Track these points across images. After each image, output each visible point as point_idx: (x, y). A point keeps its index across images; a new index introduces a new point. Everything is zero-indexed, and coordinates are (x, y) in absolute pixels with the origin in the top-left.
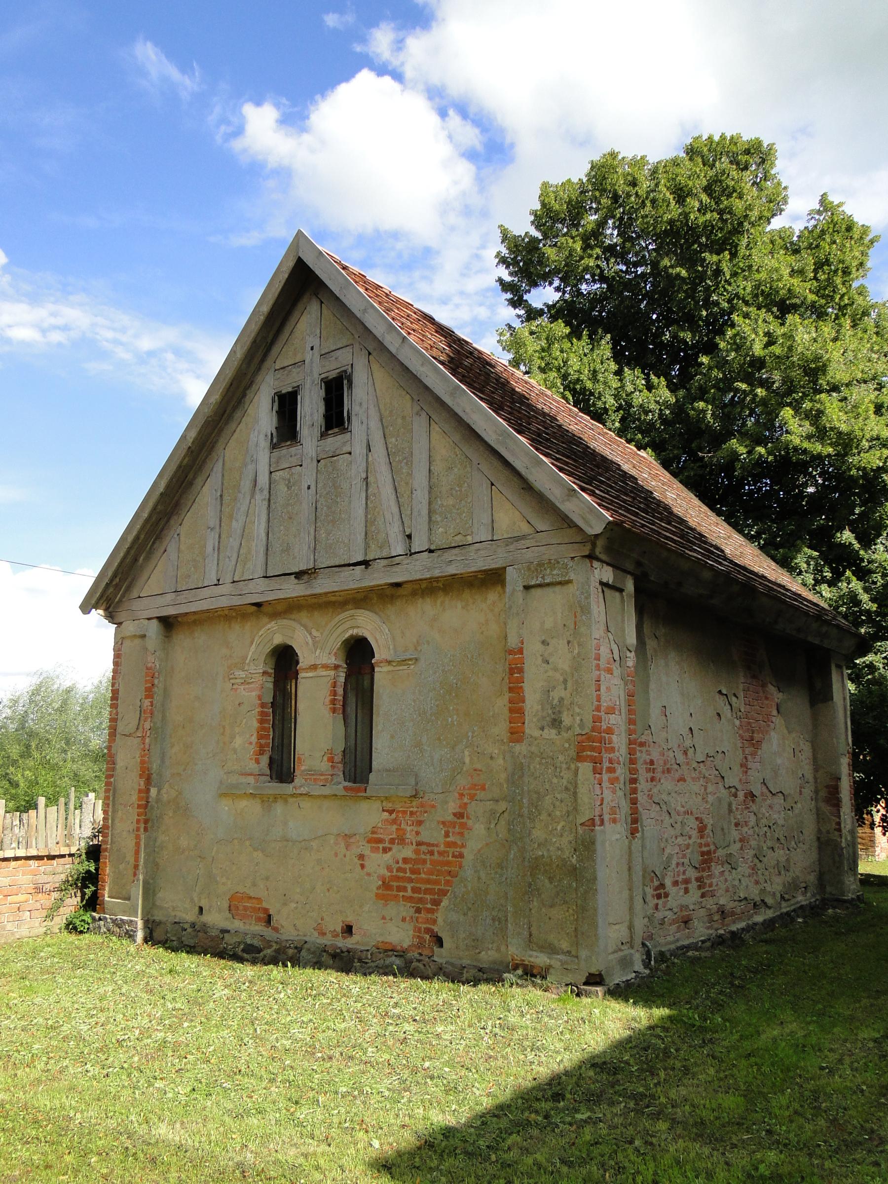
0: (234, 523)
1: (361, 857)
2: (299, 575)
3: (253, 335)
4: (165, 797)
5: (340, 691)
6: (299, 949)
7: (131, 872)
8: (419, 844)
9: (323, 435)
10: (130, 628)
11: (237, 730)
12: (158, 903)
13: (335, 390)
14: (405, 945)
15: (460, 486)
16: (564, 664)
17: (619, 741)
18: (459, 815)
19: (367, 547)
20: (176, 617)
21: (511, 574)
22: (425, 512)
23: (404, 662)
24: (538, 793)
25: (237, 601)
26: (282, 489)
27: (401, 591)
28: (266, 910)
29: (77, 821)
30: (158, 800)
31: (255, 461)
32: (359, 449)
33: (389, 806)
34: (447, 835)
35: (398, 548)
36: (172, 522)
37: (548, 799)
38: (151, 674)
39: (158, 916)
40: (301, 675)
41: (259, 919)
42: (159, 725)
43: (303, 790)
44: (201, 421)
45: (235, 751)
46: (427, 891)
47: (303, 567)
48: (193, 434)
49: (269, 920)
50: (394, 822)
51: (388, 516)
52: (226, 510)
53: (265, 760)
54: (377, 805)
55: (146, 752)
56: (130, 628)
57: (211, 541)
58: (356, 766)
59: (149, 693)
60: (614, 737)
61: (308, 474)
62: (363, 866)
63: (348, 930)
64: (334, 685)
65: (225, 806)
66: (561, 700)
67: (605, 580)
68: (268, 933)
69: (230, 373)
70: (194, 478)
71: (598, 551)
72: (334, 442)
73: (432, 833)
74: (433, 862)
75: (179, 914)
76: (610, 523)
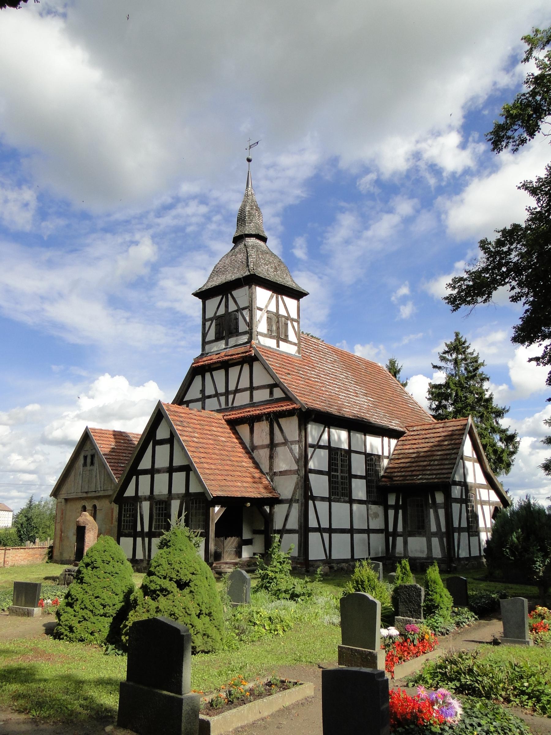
2: (86, 492)
10: (59, 500)
13: (93, 456)
29: (237, 356)
32: (95, 469)
38: (62, 510)
55: (61, 526)
56: (59, 500)
57: (73, 485)
59: (62, 514)
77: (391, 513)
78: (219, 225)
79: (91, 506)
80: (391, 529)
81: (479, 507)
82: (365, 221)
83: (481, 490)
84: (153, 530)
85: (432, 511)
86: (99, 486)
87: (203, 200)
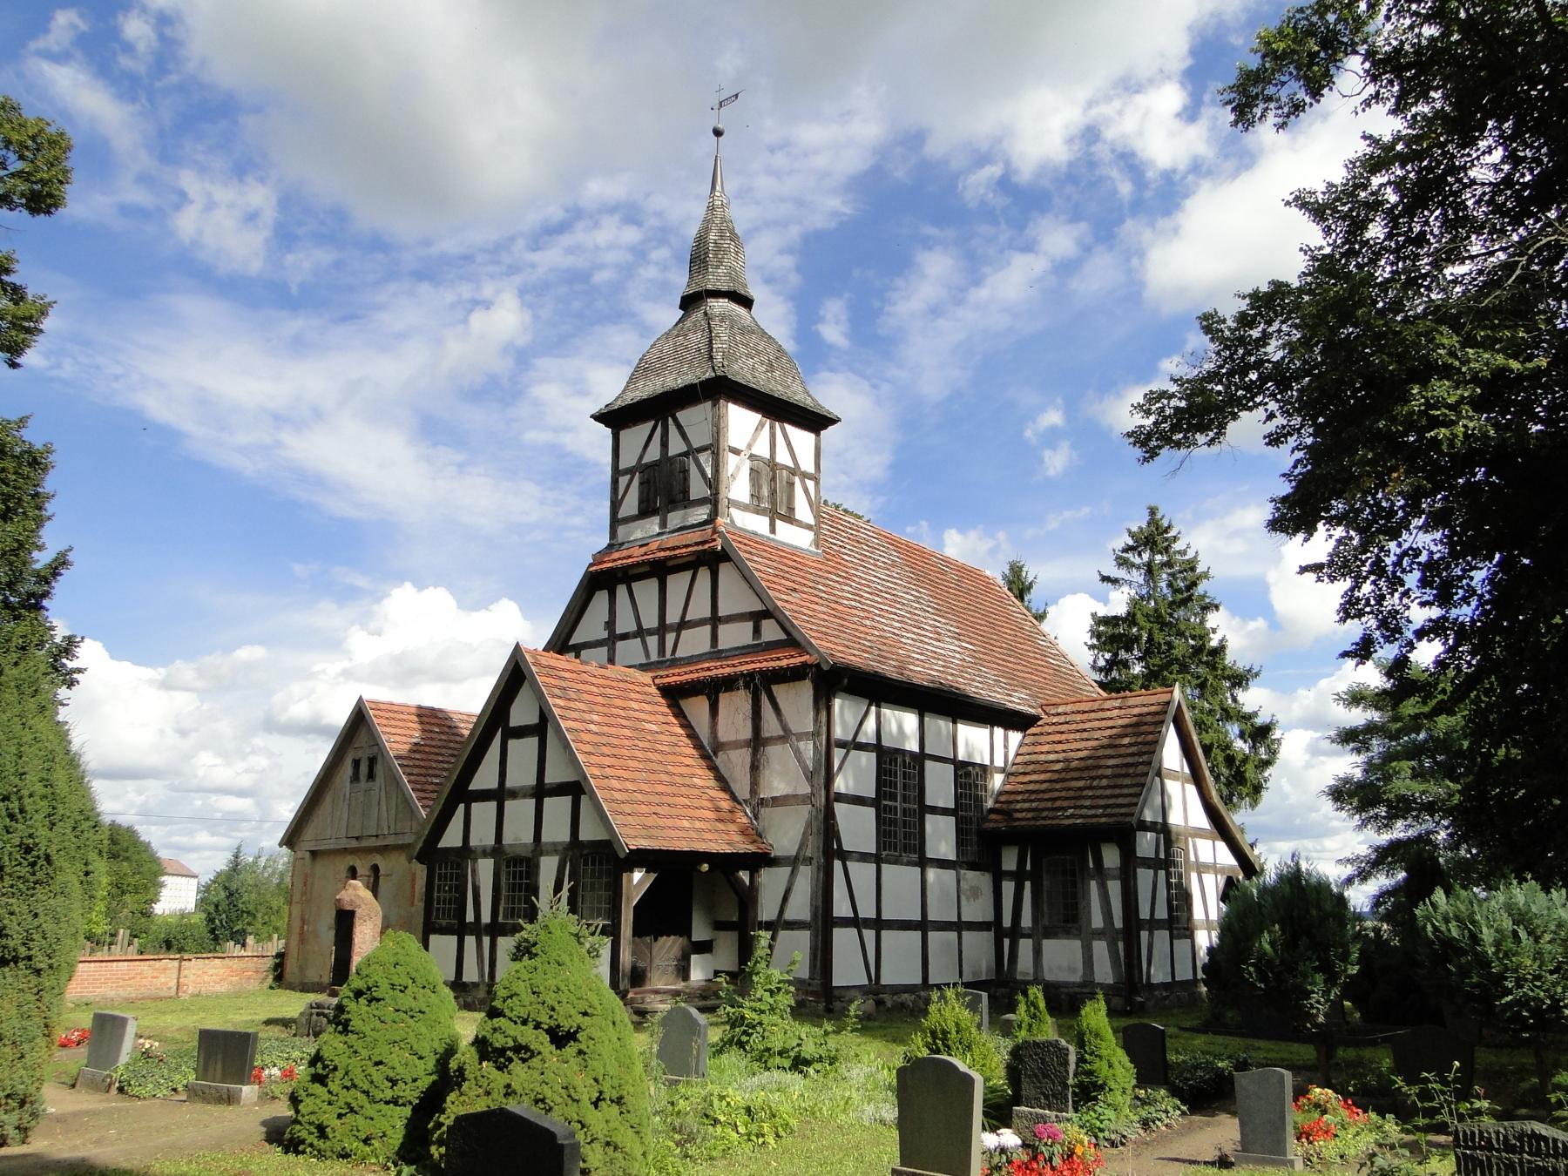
2: (357, 838)
13: (372, 761)
72: (370, 784)
77: (1008, 888)
78: (665, 268)
80: (1007, 922)
81: (1194, 876)
82: (974, 269)
83: (1199, 841)
84: (500, 919)
85: (1093, 885)
87: (630, 214)
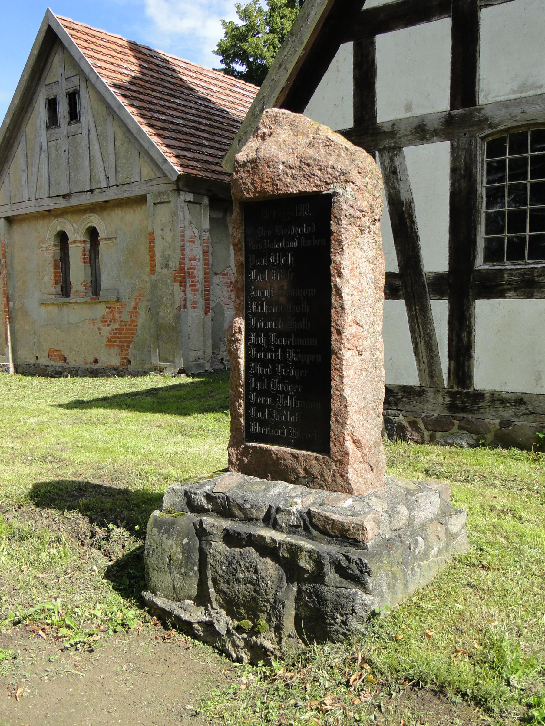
0: (34, 169)
1: (99, 329)
2: (64, 196)
3: (32, 66)
4: (17, 307)
5: (88, 253)
6: (77, 371)
7: (5, 342)
8: (121, 321)
9: (69, 123)
11: (45, 273)
12: (19, 356)
13: (73, 97)
14: (118, 365)
15: (128, 153)
16: (169, 239)
17: (199, 274)
18: (135, 308)
19: (91, 183)
20: (13, 216)
21: (149, 197)
22: (114, 166)
23: (110, 239)
24: (161, 296)
25: (38, 209)
26: (53, 151)
27: (108, 204)
28: (63, 356)
30: (13, 308)
31: (40, 136)
32: (85, 132)
33: (109, 306)
34: (131, 317)
35: (104, 185)
36: (5, 167)
37: (165, 299)
39: (19, 362)
40: (70, 246)
41: (61, 360)
42: (10, 272)
43: (74, 300)
44: (11, 115)
45: (45, 283)
46: (125, 342)
47: (65, 192)
48: (8, 121)
49: (64, 360)
50: (111, 312)
51: (99, 167)
52: (29, 161)
53: (59, 287)
54: (104, 306)
57: (24, 179)
58: (95, 287)
60: (195, 272)
61: (63, 144)
62: (100, 333)
63: (96, 361)
64: (84, 250)
65: (43, 310)
66: (169, 255)
67: (188, 200)
68: (65, 365)
69: (22, 87)
70: (13, 143)
71: (181, 187)
72: (74, 127)
73: (125, 317)
74: (127, 329)
75: (28, 360)
76: (179, 175)
79: (83, 230)
84: (480, 263)
86: (102, 175)
